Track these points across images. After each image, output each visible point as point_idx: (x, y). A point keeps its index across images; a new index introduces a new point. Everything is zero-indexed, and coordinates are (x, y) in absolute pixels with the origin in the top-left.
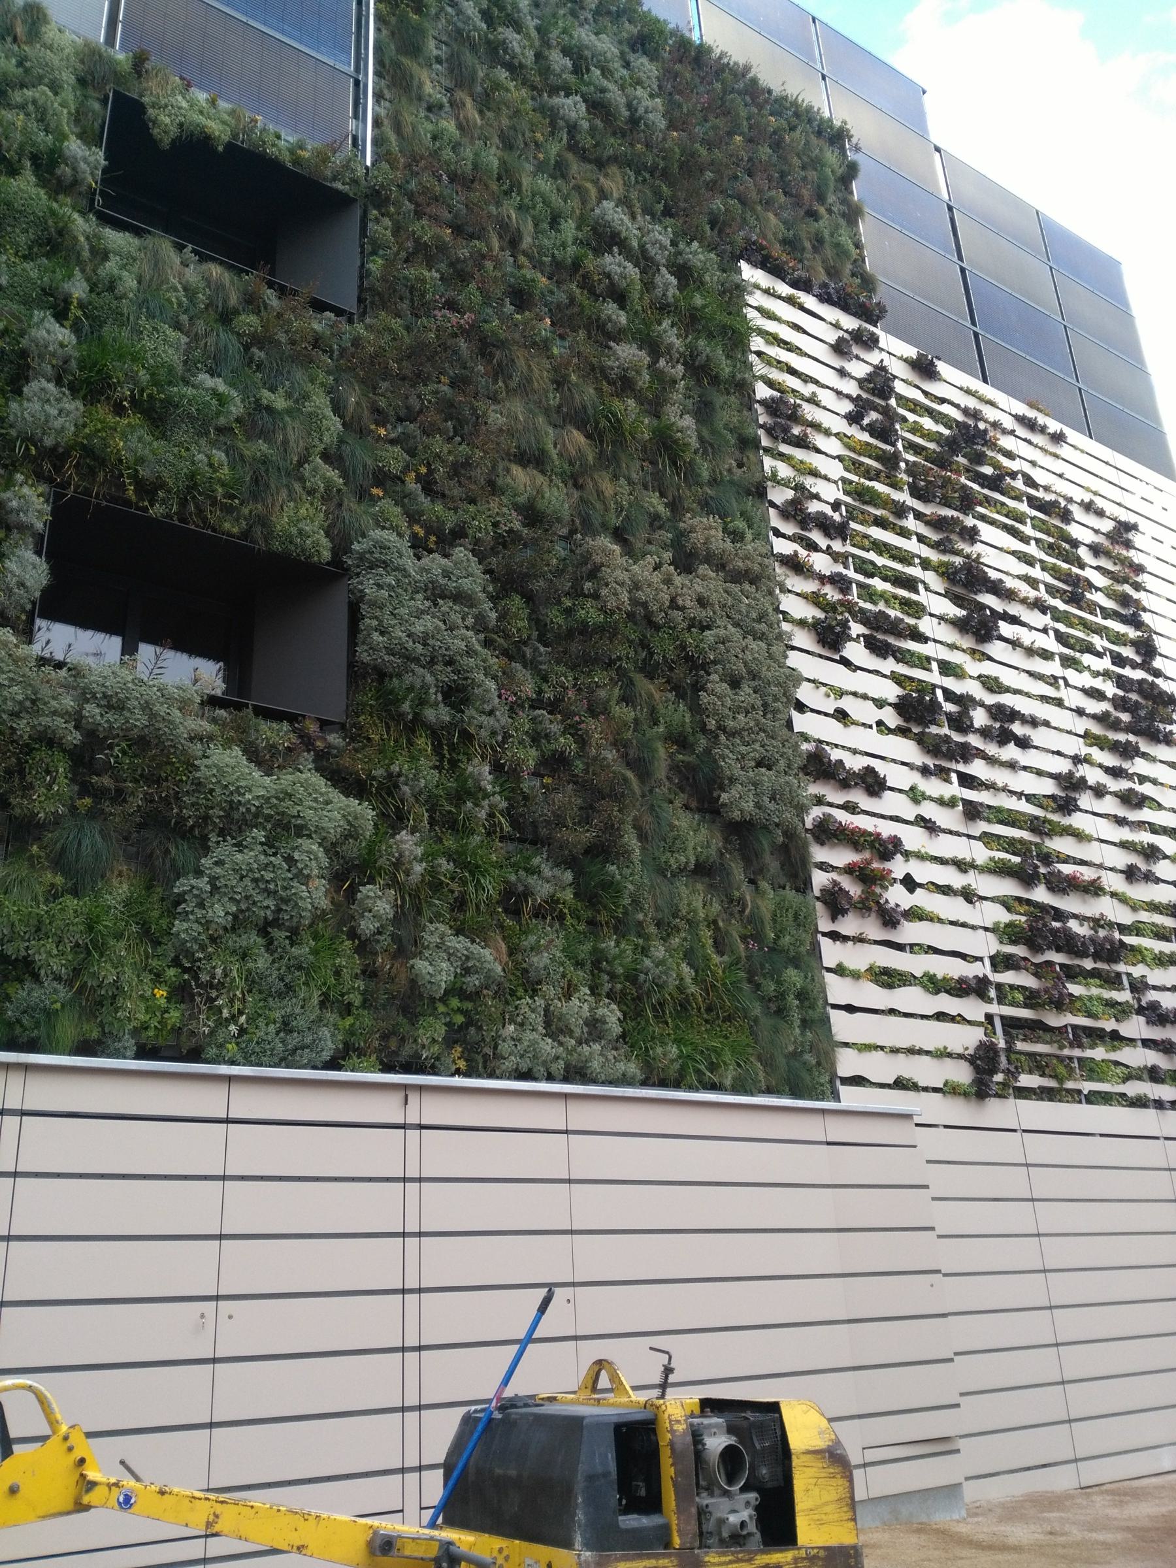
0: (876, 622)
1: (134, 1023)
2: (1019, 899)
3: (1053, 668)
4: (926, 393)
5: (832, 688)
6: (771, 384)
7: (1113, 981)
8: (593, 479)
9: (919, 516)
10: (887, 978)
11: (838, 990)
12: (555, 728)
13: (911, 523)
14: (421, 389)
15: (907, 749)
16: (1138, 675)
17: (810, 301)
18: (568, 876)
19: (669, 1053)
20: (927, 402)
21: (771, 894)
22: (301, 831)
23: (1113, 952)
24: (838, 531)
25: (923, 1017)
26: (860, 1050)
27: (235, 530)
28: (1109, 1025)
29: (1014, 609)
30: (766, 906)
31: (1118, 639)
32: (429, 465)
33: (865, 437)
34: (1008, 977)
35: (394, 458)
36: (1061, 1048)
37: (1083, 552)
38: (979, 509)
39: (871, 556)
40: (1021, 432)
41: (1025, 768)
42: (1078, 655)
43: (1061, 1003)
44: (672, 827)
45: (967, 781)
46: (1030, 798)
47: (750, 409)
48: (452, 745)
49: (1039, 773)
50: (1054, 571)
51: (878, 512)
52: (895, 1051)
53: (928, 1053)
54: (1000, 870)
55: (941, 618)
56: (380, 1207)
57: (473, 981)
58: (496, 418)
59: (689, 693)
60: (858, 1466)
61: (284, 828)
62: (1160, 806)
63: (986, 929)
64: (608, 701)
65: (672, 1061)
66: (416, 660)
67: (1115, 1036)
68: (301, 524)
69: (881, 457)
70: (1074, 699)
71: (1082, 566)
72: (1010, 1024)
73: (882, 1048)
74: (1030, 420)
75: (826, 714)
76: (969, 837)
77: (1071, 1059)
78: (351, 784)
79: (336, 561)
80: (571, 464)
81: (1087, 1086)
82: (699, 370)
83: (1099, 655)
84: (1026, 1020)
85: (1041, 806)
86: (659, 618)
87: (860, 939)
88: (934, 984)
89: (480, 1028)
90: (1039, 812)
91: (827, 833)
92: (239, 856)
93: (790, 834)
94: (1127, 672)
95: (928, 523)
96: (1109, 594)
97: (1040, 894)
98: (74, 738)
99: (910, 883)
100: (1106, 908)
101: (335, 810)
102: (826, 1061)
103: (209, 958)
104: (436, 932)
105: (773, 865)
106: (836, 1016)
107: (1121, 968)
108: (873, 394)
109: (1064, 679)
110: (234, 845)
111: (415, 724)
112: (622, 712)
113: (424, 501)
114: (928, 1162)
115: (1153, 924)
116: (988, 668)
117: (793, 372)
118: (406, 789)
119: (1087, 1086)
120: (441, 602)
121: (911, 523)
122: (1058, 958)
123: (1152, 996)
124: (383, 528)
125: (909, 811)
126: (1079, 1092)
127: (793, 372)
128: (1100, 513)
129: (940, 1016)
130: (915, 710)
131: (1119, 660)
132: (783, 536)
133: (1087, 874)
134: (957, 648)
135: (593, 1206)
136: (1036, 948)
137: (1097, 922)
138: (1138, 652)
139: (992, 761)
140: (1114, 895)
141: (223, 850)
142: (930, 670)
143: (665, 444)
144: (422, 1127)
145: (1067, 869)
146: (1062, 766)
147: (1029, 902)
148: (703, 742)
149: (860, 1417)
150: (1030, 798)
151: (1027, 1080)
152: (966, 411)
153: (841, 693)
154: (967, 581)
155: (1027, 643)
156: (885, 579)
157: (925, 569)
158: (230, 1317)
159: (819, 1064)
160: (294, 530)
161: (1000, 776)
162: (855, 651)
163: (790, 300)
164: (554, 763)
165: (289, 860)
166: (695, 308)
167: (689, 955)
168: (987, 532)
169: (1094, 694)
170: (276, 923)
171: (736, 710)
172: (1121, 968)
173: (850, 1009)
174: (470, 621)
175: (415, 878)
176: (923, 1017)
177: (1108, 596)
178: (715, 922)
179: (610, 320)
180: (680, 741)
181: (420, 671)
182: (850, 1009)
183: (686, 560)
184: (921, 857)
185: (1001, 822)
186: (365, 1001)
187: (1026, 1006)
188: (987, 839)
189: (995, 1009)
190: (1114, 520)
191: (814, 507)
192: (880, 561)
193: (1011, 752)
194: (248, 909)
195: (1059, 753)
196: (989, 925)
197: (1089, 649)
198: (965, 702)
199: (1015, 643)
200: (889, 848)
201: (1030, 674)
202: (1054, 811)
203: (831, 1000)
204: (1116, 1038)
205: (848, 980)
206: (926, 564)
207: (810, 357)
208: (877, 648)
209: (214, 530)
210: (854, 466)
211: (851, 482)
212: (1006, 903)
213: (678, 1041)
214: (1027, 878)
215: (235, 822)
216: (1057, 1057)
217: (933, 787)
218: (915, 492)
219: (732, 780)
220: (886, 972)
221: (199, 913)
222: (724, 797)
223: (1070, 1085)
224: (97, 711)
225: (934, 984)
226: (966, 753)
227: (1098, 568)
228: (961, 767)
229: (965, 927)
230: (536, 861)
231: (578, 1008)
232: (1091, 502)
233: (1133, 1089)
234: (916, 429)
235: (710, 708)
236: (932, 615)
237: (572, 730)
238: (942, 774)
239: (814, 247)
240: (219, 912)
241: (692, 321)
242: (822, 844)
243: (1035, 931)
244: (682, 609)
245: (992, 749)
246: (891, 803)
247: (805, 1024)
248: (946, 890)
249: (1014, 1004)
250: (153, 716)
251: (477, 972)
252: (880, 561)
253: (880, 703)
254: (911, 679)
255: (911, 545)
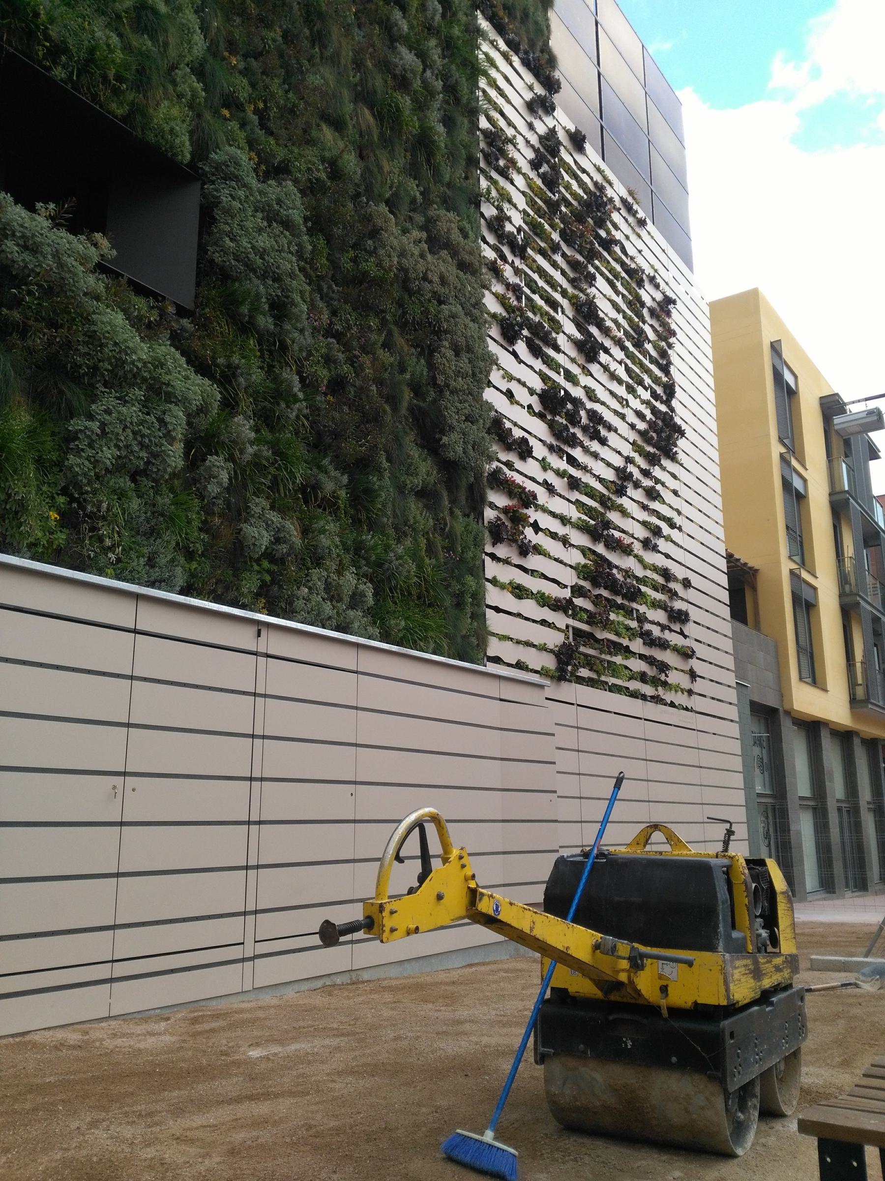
0: (536, 329)
1: (31, 540)
2: (590, 549)
3: (621, 391)
4: (576, 162)
5: (506, 372)
6: (489, 119)
7: (629, 613)
8: (375, 155)
9: (564, 255)
10: (519, 592)
11: (493, 595)
12: (341, 356)
13: (558, 258)
14: (264, 33)
16: (663, 408)
17: (516, 60)
18: (345, 479)
19: (398, 624)
20: (575, 167)
21: (461, 519)
22: (170, 398)
23: (634, 595)
24: (520, 251)
25: (534, 621)
26: (500, 639)
27: (120, 112)
28: (625, 642)
29: (608, 343)
30: (459, 528)
31: (656, 380)
32: (265, 102)
33: (539, 182)
34: (579, 602)
35: (242, 88)
37: (645, 312)
38: (596, 262)
39: (535, 276)
40: (623, 211)
41: (602, 460)
42: (636, 386)
43: (607, 625)
44: (409, 456)
45: (572, 461)
46: (601, 480)
47: (474, 134)
48: (275, 350)
49: (609, 465)
50: (629, 320)
51: (543, 245)
52: (518, 642)
53: (534, 646)
54: (583, 528)
55: (569, 337)
56: (236, 713)
57: (284, 548)
58: (313, 80)
59: (428, 352)
61: (158, 392)
62: (664, 502)
63: (571, 567)
64: (374, 344)
65: (399, 630)
66: (254, 271)
67: (627, 649)
68: (170, 121)
69: (547, 201)
70: (631, 418)
71: (644, 322)
72: (578, 633)
73: (512, 639)
74: (629, 203)
76: (568, 500)
78: (203, 368)
79: (192, 165)
80: (361, 135)
81: (612, 681)
82: (451, 89)
83: (646, 389)
84: (584, 632)
85: (607, 488)
86: (414, 286)
87: (507, 562)
88: (543, 600)
89: (281, 587)
90: (605, 491)
92: (124, 410)
93: (478, 476)
94: (657, 404)
95: (569, 262)
96: (655, 347)
97: (600, 549)
99: (536, 527)
100: (629, 563)
101: (198, 388)
102: (482, 644)
103: (95, 492)
104: (259, 504)
105: (462, 496)
106: (489, 613)
107: (635, 605)
108: (547, 151)
109: (627, 400)
110: (118, 398)
111: (246, 328)
112: (385, 356)
113: (260, 133)
115: (653, 580)
117: (502, 114)
118: (241, 380)
119: (612, 681)
120: (274, 224)
121: (558, 258)
122: (605, 593)
123: (647, 627)
124: (231, 145)
126: (606, 683)
127: (502, 114)
128: (657, 286)
129: (543, 622)
130: (552, 402)
131: (654, 395)
134: (576, 363)
135: (372, 729)
136: (595, 584)
137: (627, 573)
138: (665, 392)
139: (586, 450)
140: (636, 556)
141: (109, 400)
142: (559, 373)
143: (424, 143)
144: (268, 656)
145: (617, 534)
146: (618, 462)
147: (594, 552)
148: (432, 394)
149: (504, 885)
150: (601, 480)
151: (584, 673)
152: (596, 184)
154: (586, 313)
155: (612, 369)
156: (541, 297)
157: (564, 297)
158: (134, 790)
159: (478, 645)
160: (167, 128)
162: (521, 347)
163: (505, 56)
164: (337, 385)
165: (161, 421)
166: (451, 38)
167: (414, 554)
169: (640, 415)
170: (145, 473)
171: (458, 373)
172: (635, 605)
173: (497, 610)
174: (294, 248)
175: (247, 457)
176: (534, 621)
177: (654, 347)
178: (427, 533)
179: (396, 25)
180: (417, 390)
181: (257, 282)
182: (497, 610)
183: (436, 242)
184: (545, 510)
185: (586, 494)
186: (206, 550)
187: (587, 623)
188: (578, 504)
189: (571, 622)
190: (663, 293)
191: (509, 228)
192: (541, 283)
193: (595, 446)
194: (126, 457)
195: (619, 453)
197: (641, 383)
198: (576, 402)
199: (606, 368)
200: (528, 500)
203: (489, 602)
204: (627, 652)
206: (564, 293)
207: (513, 106)
208: (536, 352)
209: (101, 107)
210: (531, 203)
211: (529, 215)
213: (407, 619)
214: (595, 534)
215: (121, 377)
216: (598, 658)
218: (563, 234)
219: (452, 428)
221: (90, 452)
222: (445, 439)
223: (603, 678)
224: (16, 248)
225: (543, 600)
226: (573, 442)
227: (651, 326)
229: (559, 564)
230: (326, 462)
231: (350, 580)
232: (654, 277)
233: (634, 685)
234: (568, 187)
235: (441, 367)
236: (565, 333)
237: (352, 361)
238: (559, 452)
239: (522, 18)
240: (108, 454)
241: (448, 46)
242: (492, 489)
243: (597, 573)
244: (430, 282)
245: (587, 442)
246: (531, 467)
247: (474, 616)
248: (554, 536)
249: (581, 620)
250: (61, 265)
251: (285, 542)
252: (541, 283)
253: (532, 392)
254: (550, 378)
255: (557, 276)
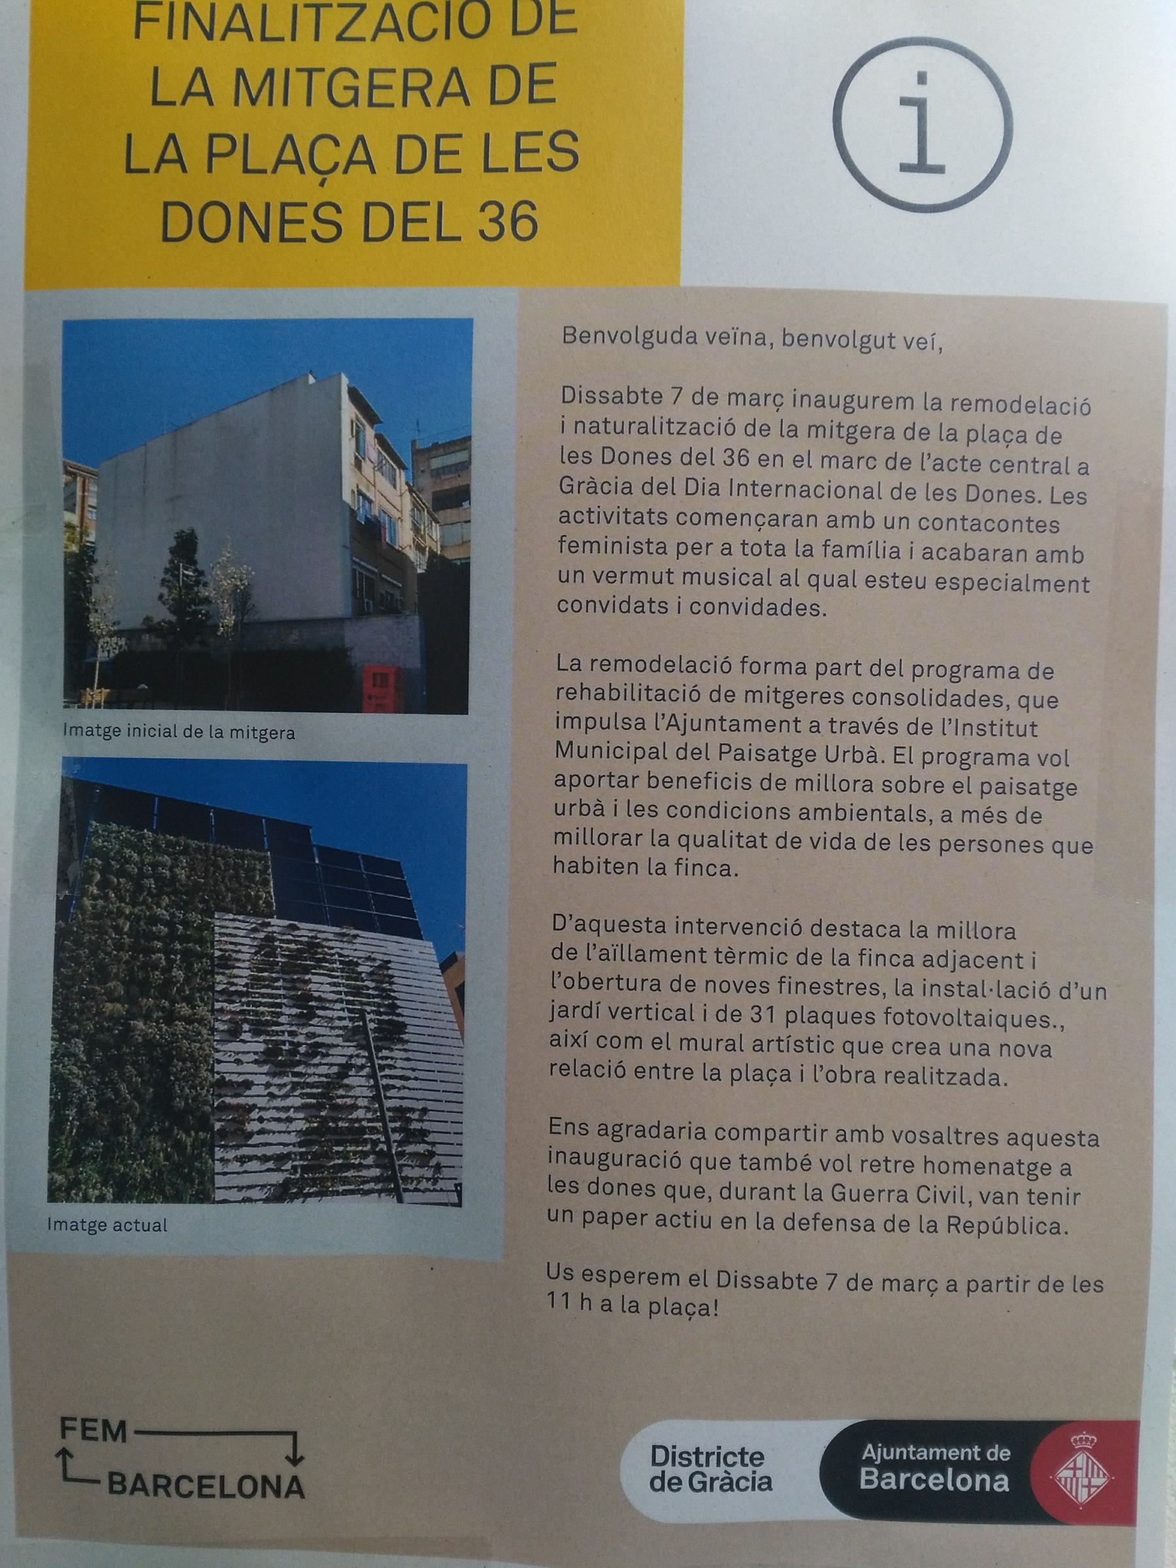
45: (295, 1074)
50: (347, 986)
60: (218, 1174)
99: (261, 1120)
114: (487, 136)
128: (374, 960)
130: (269, 1056)
146: (343, 1060)
168: (315, 978)
238: (284, 1074)
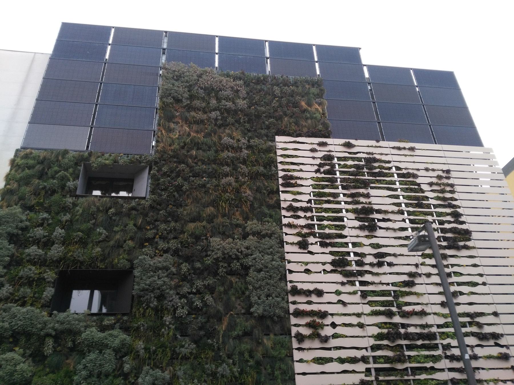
2: (386, 323)
5: (303, 262)
15: (338, 278)
25: (338, 373)
28: (429, 365)
33: (323, 175)
36: (402, 377)
39: (323, 214)
43: (401, 359)
45: (362, 283)
46: (393, 284)
63: (369, 337)
75: (301, 272)
77: (409, 380)
88: (342, 361)
91: (298, 314)
96: (438, 198)
97: (397, 319)
98: (54, 333)
99: (334, 325)
116: (374, 241)
117: (293, 164)
125: (334, 298)
129: (345, 372)
132: (287, 217)
133: (418, 308)
153: (307, 264)
161: (376, 279)
171: (258, 281)
173: (304, 374)
182: (304, 374)
192: (326, 215)
193: (386, 269)
196: (370, 335)
201: (395, 238)
202: (404, 287)
204: (433, 370)
205: (305, 364)
208: (323, 245)
211: (315, 192)
212: (379, 325)
214: (390, 314)
217: (349, 288)
220: (321, 358)
225: (342, 361)
228: (360, 278)
243: (391, 334)
246: (326, 298)
252: (326, 215)
